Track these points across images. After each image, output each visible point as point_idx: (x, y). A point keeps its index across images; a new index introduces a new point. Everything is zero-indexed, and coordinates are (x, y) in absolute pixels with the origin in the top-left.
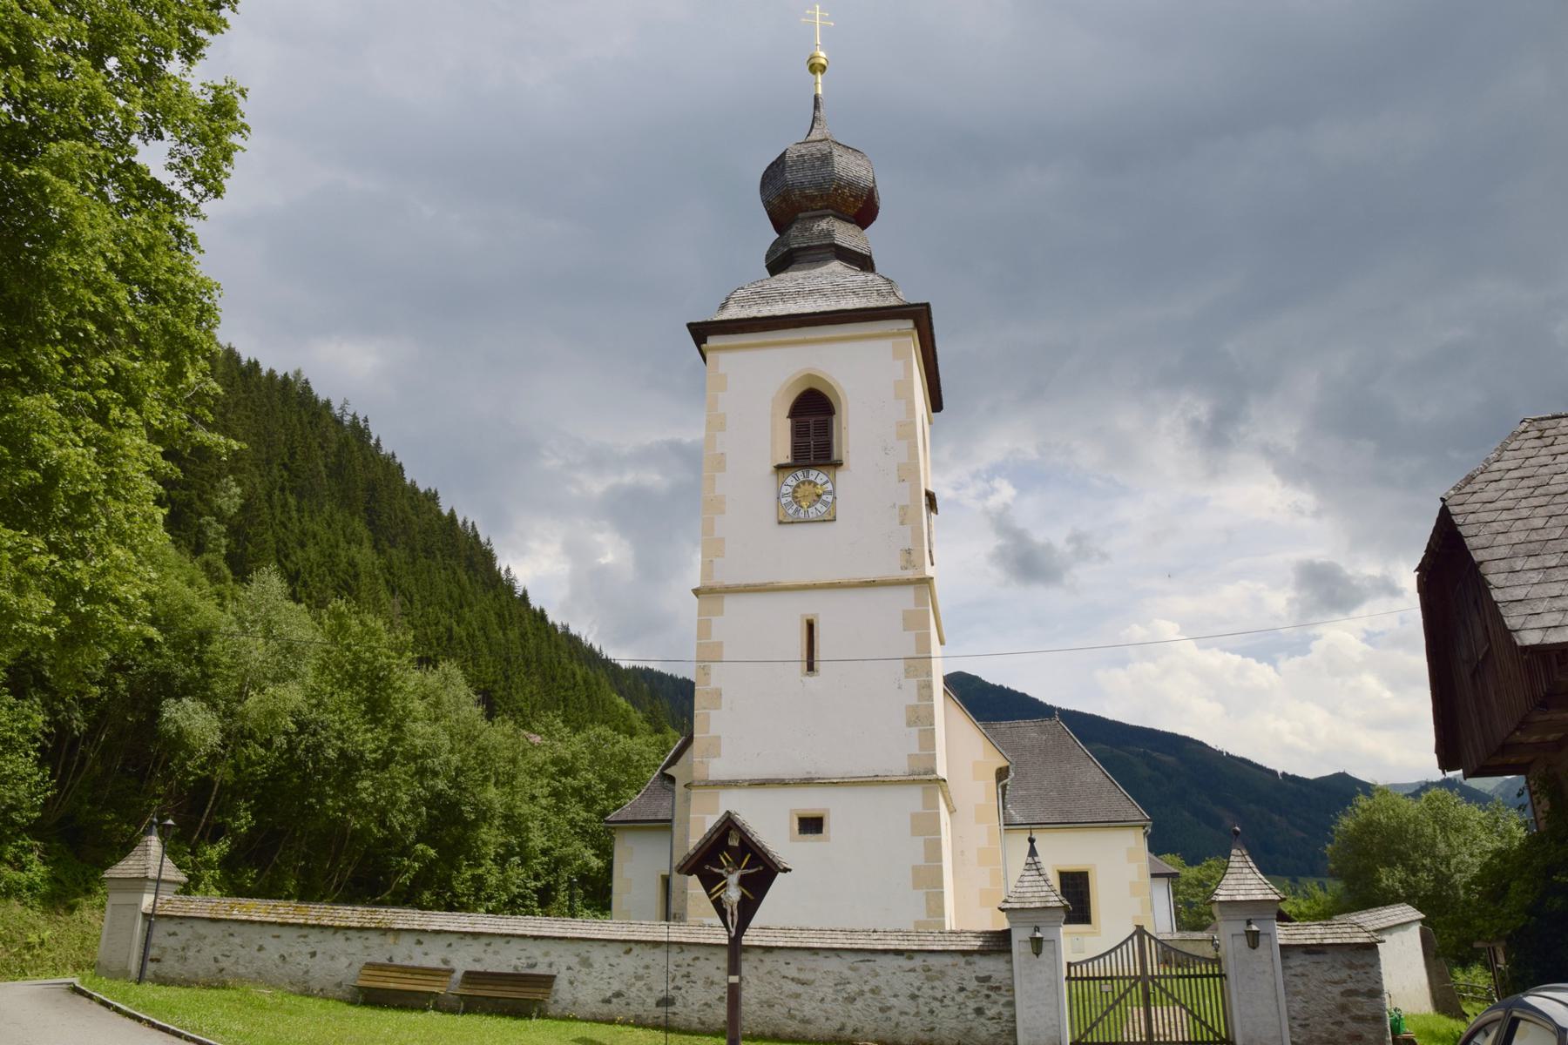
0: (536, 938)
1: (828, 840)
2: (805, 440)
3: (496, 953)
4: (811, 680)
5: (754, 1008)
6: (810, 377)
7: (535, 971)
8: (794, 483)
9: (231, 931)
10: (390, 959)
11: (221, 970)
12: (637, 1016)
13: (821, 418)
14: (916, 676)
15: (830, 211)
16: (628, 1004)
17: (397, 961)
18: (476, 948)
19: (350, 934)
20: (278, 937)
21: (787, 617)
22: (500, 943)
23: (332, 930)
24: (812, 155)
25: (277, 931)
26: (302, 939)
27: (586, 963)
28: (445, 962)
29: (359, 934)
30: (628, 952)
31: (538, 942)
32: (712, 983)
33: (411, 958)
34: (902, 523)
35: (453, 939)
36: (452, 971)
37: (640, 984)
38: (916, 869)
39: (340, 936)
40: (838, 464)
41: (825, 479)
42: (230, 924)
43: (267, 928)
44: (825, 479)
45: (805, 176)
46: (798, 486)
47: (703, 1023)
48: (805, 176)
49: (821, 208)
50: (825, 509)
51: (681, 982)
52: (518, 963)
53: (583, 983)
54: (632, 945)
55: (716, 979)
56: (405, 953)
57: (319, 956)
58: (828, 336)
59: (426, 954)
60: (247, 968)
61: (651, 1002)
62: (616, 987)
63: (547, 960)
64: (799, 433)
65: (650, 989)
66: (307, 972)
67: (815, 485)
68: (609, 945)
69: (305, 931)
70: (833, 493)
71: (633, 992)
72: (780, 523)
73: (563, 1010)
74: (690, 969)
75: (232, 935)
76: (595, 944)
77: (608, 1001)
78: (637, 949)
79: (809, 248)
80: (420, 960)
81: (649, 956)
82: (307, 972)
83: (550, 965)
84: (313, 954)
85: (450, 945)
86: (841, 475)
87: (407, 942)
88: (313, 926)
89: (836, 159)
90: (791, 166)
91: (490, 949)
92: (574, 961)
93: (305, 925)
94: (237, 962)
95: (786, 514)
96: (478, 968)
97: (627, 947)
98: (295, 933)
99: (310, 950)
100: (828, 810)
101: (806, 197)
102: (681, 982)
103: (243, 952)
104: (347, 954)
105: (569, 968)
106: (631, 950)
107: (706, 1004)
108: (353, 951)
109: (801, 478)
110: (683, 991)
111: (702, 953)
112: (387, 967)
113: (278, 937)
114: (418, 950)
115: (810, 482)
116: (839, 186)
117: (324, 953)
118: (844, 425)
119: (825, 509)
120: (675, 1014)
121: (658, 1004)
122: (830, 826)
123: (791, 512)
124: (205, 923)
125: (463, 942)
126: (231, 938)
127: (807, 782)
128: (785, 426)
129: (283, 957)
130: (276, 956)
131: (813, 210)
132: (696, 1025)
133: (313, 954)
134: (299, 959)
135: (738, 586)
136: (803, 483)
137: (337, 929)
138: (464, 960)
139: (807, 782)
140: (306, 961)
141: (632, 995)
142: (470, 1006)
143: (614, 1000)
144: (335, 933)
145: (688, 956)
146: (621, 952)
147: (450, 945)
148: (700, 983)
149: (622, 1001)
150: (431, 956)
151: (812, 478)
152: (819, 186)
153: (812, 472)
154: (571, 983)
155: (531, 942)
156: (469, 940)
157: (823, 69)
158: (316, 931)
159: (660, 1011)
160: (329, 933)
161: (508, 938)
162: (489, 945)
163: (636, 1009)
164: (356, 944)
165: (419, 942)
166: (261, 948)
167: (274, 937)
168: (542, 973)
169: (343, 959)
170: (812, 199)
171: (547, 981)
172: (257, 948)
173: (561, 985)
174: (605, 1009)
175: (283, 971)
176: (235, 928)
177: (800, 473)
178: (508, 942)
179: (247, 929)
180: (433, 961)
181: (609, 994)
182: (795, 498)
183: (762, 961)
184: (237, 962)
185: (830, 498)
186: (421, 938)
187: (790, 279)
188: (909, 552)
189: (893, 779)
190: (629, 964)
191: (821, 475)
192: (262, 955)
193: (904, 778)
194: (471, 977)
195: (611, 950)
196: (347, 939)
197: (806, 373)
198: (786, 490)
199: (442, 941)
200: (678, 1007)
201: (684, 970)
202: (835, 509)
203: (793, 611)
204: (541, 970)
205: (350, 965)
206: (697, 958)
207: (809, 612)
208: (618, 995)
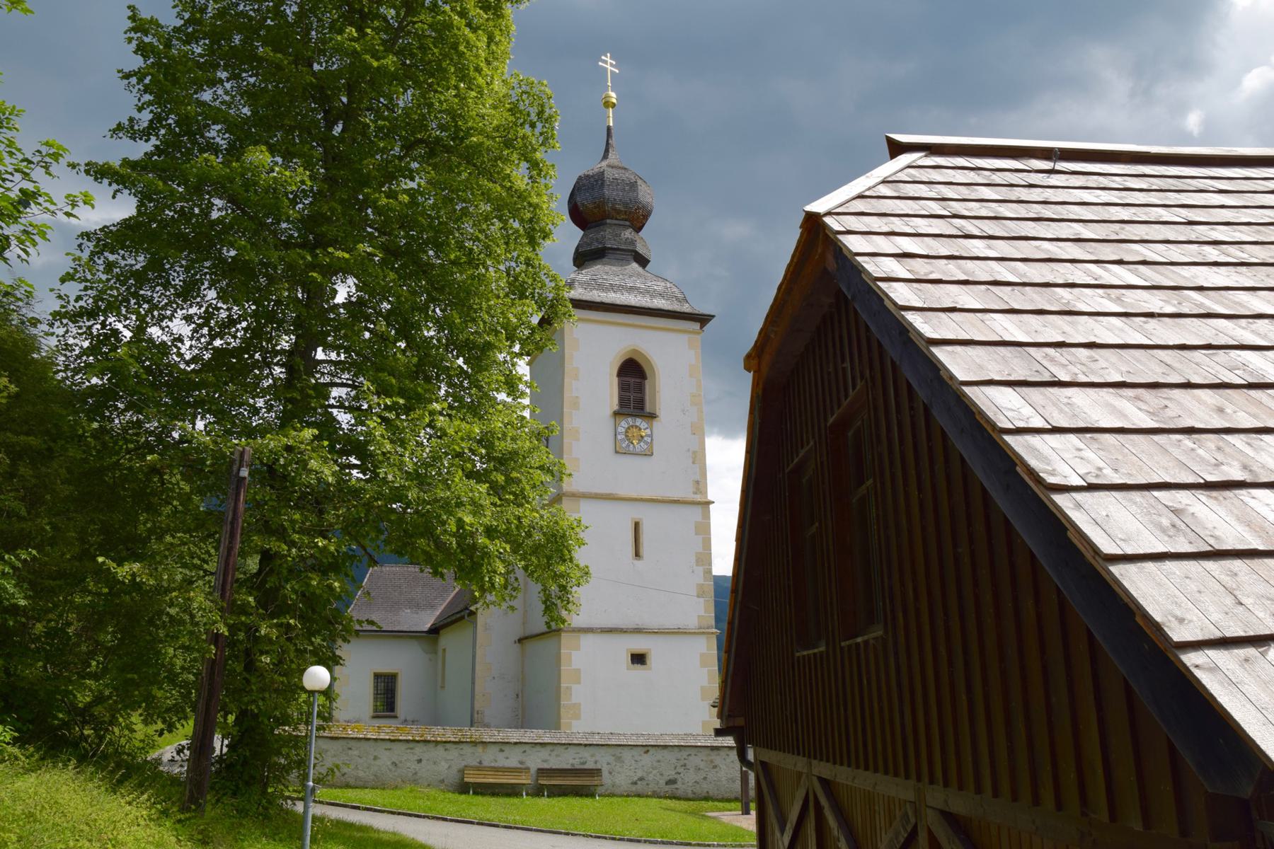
0: (586, 745)
1: (650, 669)
2: (628, 394)
3: (557, 756)
4: (638, 563)
5: (724, 783)
6: (635, 351)
7: (586, 767)
8: (626, 426)
9: (349, 746)
10: (480, 763)
11: (343, 775)
12: (654, 792)
13: (638, 380)
14: (703, 565)
15: (628, 223)
16: (648, 784)
17: (486, 763)
18: (544, 753)
19: (448, 746)
20: (390, 749)
21: (622, 518)
22: (561, 749)
23: (434, 744)
24: (623, 180)
25: (389, 745)
26: (409, 751)
27: (619, 759)
28: (521, 763)
29: (455, 746)
30: (647, 752)
31: (587, 748)
32: (699, 769)
33: (496, 761)
34: (693, 463)
35: (527, 748)
36: (528, 769)
37: (654, 772)
38: (703, 688)
39: (440, 748)
40: (652, 416)
41: (646, 426)
42: (349, 741)
43: (380, 743)
44: (646, 426)
45: (618, 195)
46: (629, 428)
47: (694, 794)
48: (618, 195)
49: (622, 220)
50: (646, 447)
51: (681, 770)
52: (574, 762)
53: (619, 773)
54: (650, 748)
55: (701, 767)
56: (490, 757)
57: (424, 762)
58: (643, 324)
59: (507, 758)
60: (365, 772)
61: (662, 782)
62: (640, 774)
63: (593, 759)
64: (623, 388)
65: (662, 775)
66: (416, 773)
67: (640, 429)
68: (635, 748)
69: (411, 745)
70: (651, 436)
71: (651, 777)
72: (617, 452)
73: (606, 790)
74: (686, 761)
75: (350, 749)
76: (626, 748)
77: (635, 783)
78: (652, 751)
79: (618, 249)
80: (502, 762)
81: (660, 754)
82: (416, 773)
83: (596, 762)
84: (420, 761)
85: (525, 752)
86: (656, 423)
87: (492, 751)
88: (418, 742)
89: (639, 187)
90: (609, 185)
91: (555, 753)
92: (611, 759)
93: (414, 741)
94: (357, 768)
95: (621, 447)
96: (546, 766)
97: (646, 749)
98: (402, 747)
99: (416, 758)
100: (650, 650)
101: (615, 209)
102: (681, 770)
103: (360, 761)
104: (446, 760)
105: (608, 764)
106: (648, 751)
107: (696, 782)
108: (452, 758)
109: (631, 423)
110: (682, 775)
111: (693, 751)
112: (480, 768)
113: (390, 749)
114: (501, 756)
115: (637, 427)
116: (638, 208)
117: (428, 760)
118: (657, 389)
119: (646, 447)
120: (677, 789)
121: (667, 784)
122: (652, 660)
123: (624, 445)
124: (327, 740)
125: (534, 750)
126: (350, 751)
127: (638, 631)
128: (615, 380)
129: (394, 764)
130: (389, 763)
131: (616, 219)
132: (690, 795)
133: (420, 761)
134: (409, 764)
135: (591, 494)
136: (632, 426)
137: (437, 743)
138: (536, 760)
139: (638, 631)
140: (414, 766)
141: (651, 779)
142: (538, 792)
143: (639, 782)
144: (436, 746)
145: (684, 753)
146: (642, 753)
147: (525, 752)
148: (692, 770)
149: (645, 783)
150: (512, 759)
151: (638, 424)
152: (626, 205)
153: (637, 419)
154: (610, 773)
155: (583, 748)
156: (538, 748)
157: (614, 105)
158: (421, 745)
159: (667, 788)
160: (431, 745)
161: (566, 746)
162: (552, 751)
163: (653, 787)
164: (454, 753)
165: (502, 751)
166: (376, 758)
167: (386, 749)
168: (591, 767)
169: (443, 763)
170: (619, 212)
171: (596, 772)
172: (372, 757)
173: (605, 773)
174: (634, 788)
175: (396, 774)
176: (352, 743)
177: (630, 419)
178: (567, 749)
179: (364, 744)
180: (513, 762)
181: (635, 779)
182: (627, 436)
183: (728, 755)
184: (357, 768)
185: (649, 440)
186: (503, 747)
187: (598, 270)
188: (698, 482)
189: (688, 631)
190: (647, 760)
191: (644, 423)
192: (378, 762)
193: (696, 631)
194: (542, 772)
195: (635, 752)
196: (446, 750)
197: (632, 348)
198: (620, 429)
199: (519, 749)
200: (679, 785)
201: (682, 762)
202: (652, 447)
203: (627, 514)
204: (590, 765)
205: (449, 767)
206: (690, 755)
207: (637, 517)
208: (641, 779)
